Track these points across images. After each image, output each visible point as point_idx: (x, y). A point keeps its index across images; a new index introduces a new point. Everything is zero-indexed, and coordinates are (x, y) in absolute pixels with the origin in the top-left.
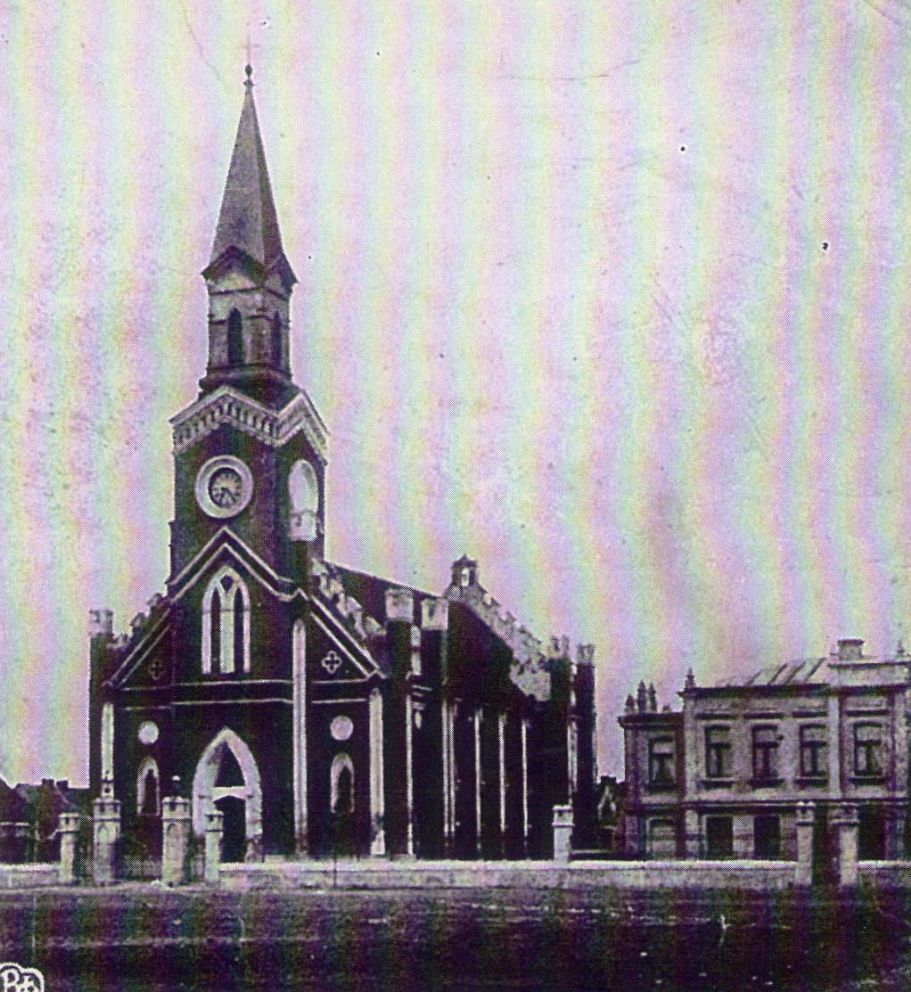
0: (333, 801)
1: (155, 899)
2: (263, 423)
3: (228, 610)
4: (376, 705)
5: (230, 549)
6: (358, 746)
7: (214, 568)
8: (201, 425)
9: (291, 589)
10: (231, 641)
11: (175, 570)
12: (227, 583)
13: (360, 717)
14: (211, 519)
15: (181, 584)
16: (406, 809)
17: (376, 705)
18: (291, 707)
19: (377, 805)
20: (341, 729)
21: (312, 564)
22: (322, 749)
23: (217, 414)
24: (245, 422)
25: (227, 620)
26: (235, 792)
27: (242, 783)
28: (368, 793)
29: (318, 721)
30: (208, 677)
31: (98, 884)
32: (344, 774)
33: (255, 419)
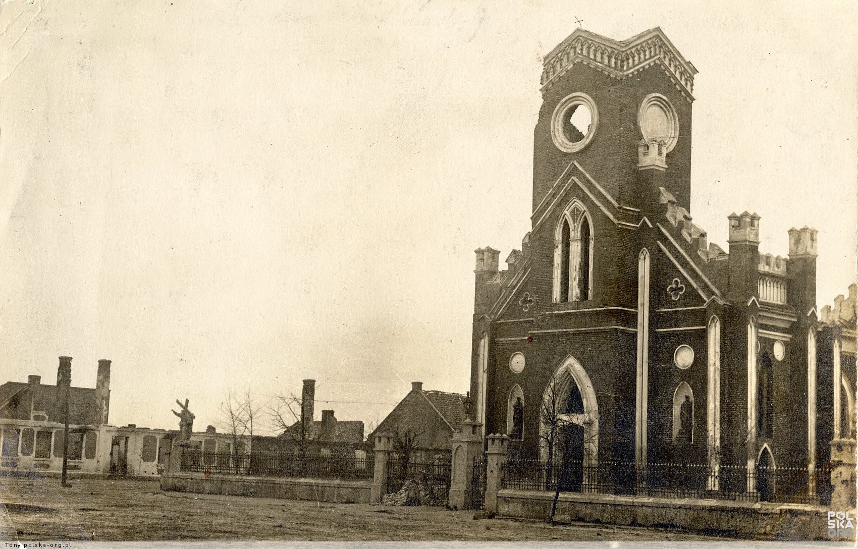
1: (226, 487)
2: (610, 57)
3: (576, 240)
4: (714, 334)
7: (564, 201)
9: (638, 218)
11: (535, 206)
13: (699, 342)
14: (566, 154)
16: (552, 373)
17: (714, 334)
19: (714, 430)
20: (685, 357)
22: (663, 377)
23: (572, 54)
24: (595, 60)
26: (578, 419)
27: (581, 411)
29: (661, 351)
31: (452, 507)
32: (686, 406)
33: (602, 54)
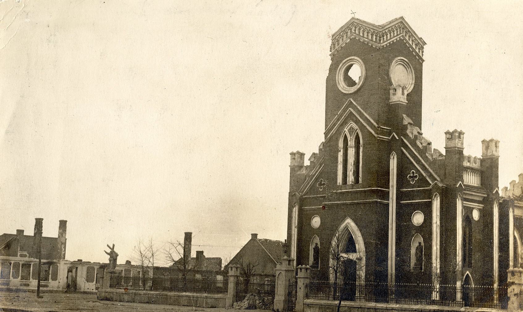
0: (412, 264)
2: (372, 35)
4: (436, 204)
5: (352, 110)
6: (425, 229)
8: (341, 41)
9: (389, 133)
10: (293, 221)
12: (351, 130)
13: (427, 209)
15: (329, 132)
17: (436, 204)
18: (388, 192)
19: (436, 263)
20: (418, 219)
21: (403, 119)
23: (349, 33)
24: (363, 37)
25: (351, 152)
26: (353, 256)
28: (431, 258)
29: (404, 214)
30: (340, 187)
32: (419, 249)
33: (368, 33)
